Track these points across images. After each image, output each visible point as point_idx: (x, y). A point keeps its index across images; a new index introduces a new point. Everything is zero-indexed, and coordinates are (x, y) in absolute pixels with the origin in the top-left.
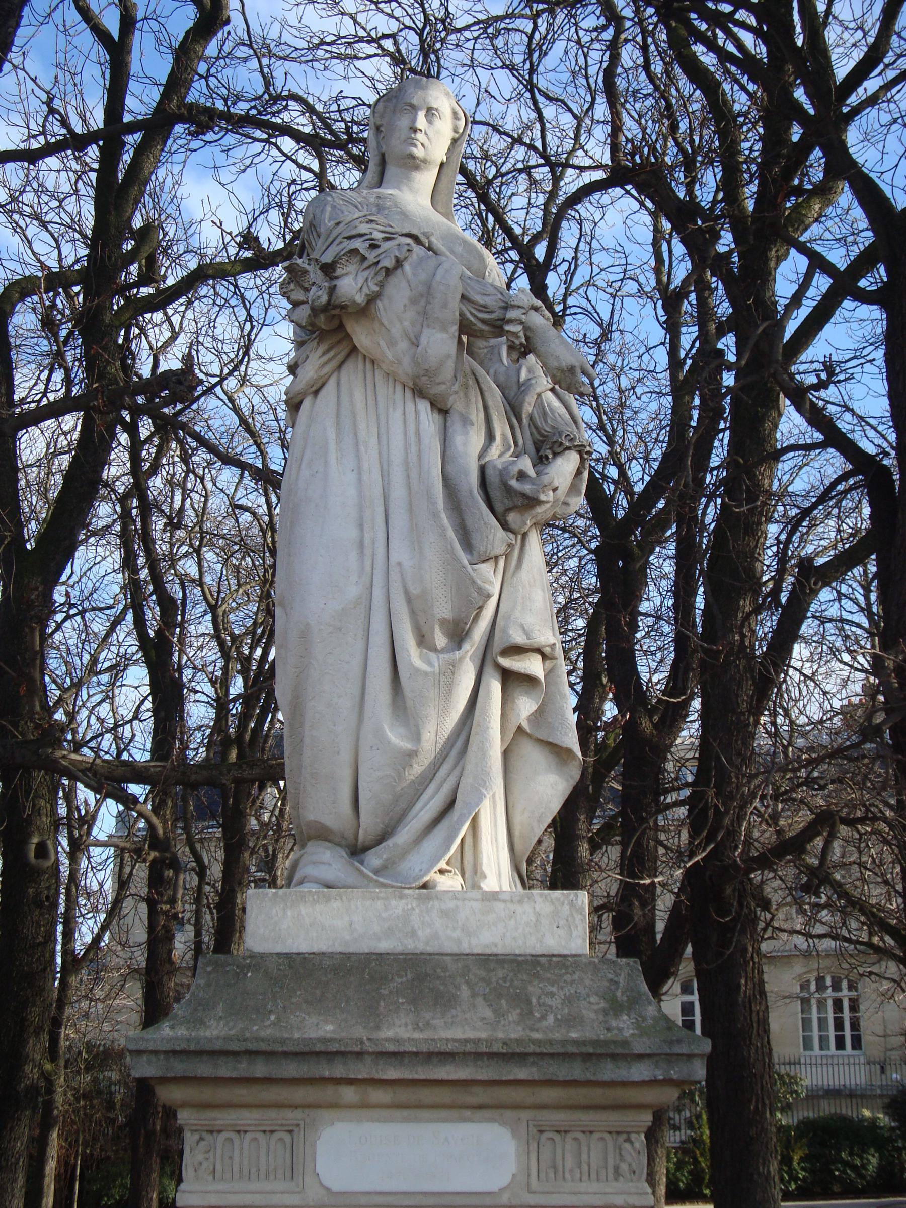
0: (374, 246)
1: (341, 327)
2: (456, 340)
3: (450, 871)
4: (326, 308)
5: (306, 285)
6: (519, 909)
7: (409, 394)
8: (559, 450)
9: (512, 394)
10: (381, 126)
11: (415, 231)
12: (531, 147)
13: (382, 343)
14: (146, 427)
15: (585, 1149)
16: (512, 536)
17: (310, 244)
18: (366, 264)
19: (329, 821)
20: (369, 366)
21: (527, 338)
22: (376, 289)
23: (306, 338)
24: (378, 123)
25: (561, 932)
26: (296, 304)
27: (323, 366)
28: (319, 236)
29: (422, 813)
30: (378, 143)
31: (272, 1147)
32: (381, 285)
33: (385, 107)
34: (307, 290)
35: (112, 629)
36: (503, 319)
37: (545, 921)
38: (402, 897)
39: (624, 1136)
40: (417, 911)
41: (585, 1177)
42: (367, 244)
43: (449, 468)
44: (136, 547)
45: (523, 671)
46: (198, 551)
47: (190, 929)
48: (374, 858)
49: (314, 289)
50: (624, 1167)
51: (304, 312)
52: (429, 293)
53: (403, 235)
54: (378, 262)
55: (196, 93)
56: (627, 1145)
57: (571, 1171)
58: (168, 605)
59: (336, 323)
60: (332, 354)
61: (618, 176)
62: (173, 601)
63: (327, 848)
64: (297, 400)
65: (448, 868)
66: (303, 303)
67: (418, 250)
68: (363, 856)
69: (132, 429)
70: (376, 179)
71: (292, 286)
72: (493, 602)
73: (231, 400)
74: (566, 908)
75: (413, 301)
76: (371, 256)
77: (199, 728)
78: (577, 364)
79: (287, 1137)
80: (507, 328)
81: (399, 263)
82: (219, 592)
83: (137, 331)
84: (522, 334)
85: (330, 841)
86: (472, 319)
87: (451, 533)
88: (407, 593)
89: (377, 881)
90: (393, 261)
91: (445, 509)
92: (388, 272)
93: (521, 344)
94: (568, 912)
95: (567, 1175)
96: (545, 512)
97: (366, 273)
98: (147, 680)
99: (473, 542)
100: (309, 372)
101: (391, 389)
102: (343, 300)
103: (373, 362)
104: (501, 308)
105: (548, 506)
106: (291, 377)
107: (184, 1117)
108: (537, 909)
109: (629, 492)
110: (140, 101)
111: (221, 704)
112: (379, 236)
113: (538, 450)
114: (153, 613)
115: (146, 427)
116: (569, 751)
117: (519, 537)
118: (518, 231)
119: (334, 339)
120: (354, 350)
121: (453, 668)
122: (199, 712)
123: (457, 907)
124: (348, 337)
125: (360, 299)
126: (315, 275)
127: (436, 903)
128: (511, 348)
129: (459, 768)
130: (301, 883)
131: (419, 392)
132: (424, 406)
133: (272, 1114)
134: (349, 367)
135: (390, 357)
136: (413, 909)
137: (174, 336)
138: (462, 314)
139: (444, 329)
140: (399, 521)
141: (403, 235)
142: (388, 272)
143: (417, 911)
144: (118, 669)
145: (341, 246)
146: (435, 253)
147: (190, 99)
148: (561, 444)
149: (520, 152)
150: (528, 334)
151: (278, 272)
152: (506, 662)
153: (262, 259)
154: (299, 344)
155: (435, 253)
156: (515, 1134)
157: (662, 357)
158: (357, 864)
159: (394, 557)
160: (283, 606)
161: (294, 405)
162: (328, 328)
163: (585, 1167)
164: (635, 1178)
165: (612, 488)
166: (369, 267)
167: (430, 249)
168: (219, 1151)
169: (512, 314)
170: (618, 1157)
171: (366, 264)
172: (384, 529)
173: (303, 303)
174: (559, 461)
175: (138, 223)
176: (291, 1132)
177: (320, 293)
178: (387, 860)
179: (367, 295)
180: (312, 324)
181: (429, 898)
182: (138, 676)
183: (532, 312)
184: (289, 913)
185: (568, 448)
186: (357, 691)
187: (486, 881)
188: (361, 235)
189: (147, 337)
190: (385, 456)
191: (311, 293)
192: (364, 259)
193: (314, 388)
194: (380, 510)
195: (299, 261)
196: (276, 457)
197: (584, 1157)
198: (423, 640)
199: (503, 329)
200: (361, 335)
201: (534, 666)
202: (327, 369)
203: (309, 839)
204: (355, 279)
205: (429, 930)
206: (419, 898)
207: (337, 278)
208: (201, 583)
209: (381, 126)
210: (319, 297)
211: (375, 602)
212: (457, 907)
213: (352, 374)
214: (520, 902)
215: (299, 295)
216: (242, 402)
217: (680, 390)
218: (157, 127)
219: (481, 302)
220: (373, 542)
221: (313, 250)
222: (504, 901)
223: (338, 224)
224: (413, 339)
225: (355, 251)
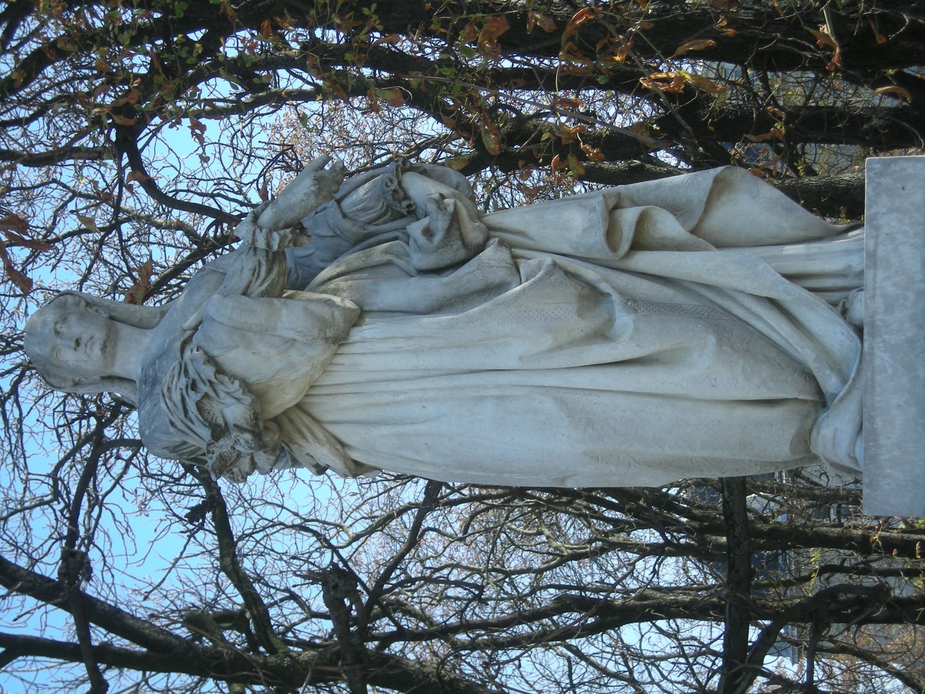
0: (194, 386)
1: (276, 420)
2: (289, 301)
3: (844, 304)
4: (258, 436)
5: (235, 456)
6: (885, 229)
7: (345, 349)
9: (344, 243)
10: (74, 381)
11: (178, 345)
12: (101, 242)
13: (292, 377)
14: (385, 626)
16: (492, 241)
17: (193, 452)
18: (212, 393)
19: (790, 432)
20: (315, 392)
21: (286, 226)
22: (237, 383)
23: (288, 456)
24: (71, 383)
26: (254, 466)
28: (185, 443)
29: (783, 334)
30: (91, 384)
32: (233, 377)
33: (55, 376)
34: (239, 455)
35: (583, 657)
36: (267, 252)
40: (886, 337)
42: (191, 393)
43: (421, 306)
44: (504, 635)
45: (634, 227)
46: (508, 574)
47: (891, 581)
48: (829, 383)
49: (238, 448)
51: (262, 458)
52: (241, 329)
53: (182, 356)
54: (210, 382)
55: (49, 568)
58: (562, 605)
59: (272, 425)
60: (304, 429)
61: (127, 144)
62: (558, 599)
63: (818, 433)
64: (352, 466)
65: (841, 304)
66: (252, 459)
67: (198, 338)
68: (827, 397)
69: (387, 639)
70: (127, 385)
71: (235, 470)
72: (560, 260)
73: (356, 538)
75: (249, 345)
76: (204, 388)
77: (686, 572)
78: (312, 175)
80: (275, 248)
82: (549, 554)
83: (290, 634)
84: (282, 232)
85: (811, 430)
86: (266, 284)
87: (487, 305)
89: (854, 380)
91: (462, 311)
96: (466, 207)
97: (222, 395)
98: (635, 625)
99: (497, 281)
100: (324, 454)
101: (339, 368)
102: (248, 415)
103: (312, 387)
104: (255, 254)
105: (459, 204)
106: (329, 472)
108: (884, 210)
109: (447, 139)
110: (58, 624)
111: (659, 551)
112: (183, 380)
113: (402, 216)
114: (571, 618)
115: (385, 626)
116: (717, 180)
117: (492, 233)
118: (186, 254)
119: (289, 427)
120: (299, 406)
122: (671, 572)
124: (285, 413)
125: (248, 399)
126: (224, 446)
127: (878, 317)
128: (295, 243)
129: (735, 295)
130: (855, 460)
131: (340, 340)
134: (315, 411)
135: (307, 368)
136: (884, 341)
137: (293, 597)
140: (476, 359)
141: (182, 356)
142: (220, 370)
143: (886, 337)
144: (628, 654)
145: (194, 418)
146: (201, 322)
147: (55, 576)
148: (395, 191)
149: (106, 253)
150: (281, 225)
151: (223, 483)
152: (625, 247)
153: (215, 504)
154: (295, 463)
155: (201, 322)
157: (312, 107)
158: (836, 401)
159: (513, 363)
160: (564, 480)
161: (356, 469)
162: (277, 436)
165: (444, 155)
166: (215, 391)
167: (196, 329)
169: (261, 244)
171: (212, 393)
172: (484, 374)
173: (252, 459)
174: (412, 193)
175: (183, 632)
177: (242, 441)
178: (831, 369)
179: (244, 393)
180: (274, 450)
181: (873, 324)
182: (630, 633)
184: (888, 471)
185: (400, 183)
186: (655, 401)
187: (854, 264)
188: (183, 400)
189: (295, 624)
190: (409, 374)
191: (242, 450)
193: (339, 447)
195: (210, 462)
196: (414, 492)
199: (277, 252)
200: (284, 399)
201: (629, 216)
202: (320, 434)
203: (808, 451)
204: (227, 406)
206: (873, 335)
207: (226, 424)
208: (540, 572)
209: (74, 381)
210: (247, 442)
211: (561, 384)
213: (328, 409)
214: (877, 228)
215: (245, 463)
216: (360, 527)
217: (341, 89)
218: (88, 611)
220: (497, 386)
221: (199, 449)
223: (172, 424)
224: (289, 344)
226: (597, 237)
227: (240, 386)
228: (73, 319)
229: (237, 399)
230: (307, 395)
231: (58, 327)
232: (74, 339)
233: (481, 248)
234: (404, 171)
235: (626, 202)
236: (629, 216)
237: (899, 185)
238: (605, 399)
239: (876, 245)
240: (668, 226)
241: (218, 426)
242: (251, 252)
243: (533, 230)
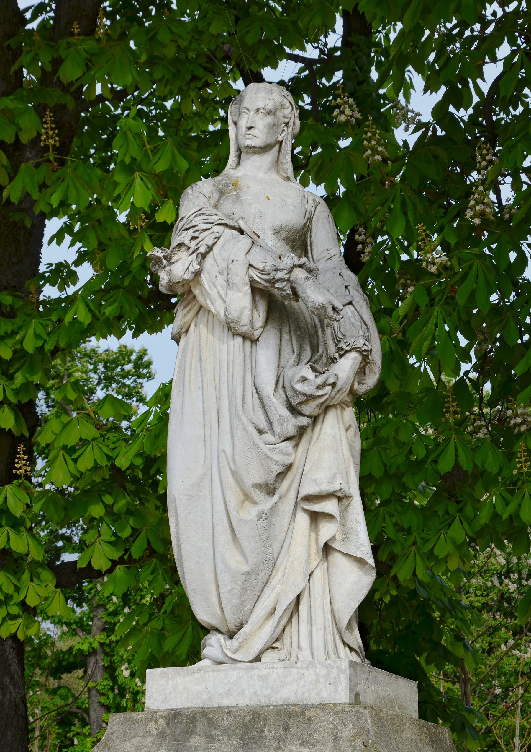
6: (306, 673)
18: (191, 251)
22: (198, 267)
25: (332, 687)
27: (185, 315)
37: (322, 680)
40: (245, 677)
60: (190, 307)
76: (193, 245)
78: (325, 302)
86: (258, 279)
88: (231, 469)
94: (335, 673)
108: (317, 671)
123: (269, 673)
127: (256, 671)
136: (243, 676)
142: (204, 256)
143: (245, 677)
148: (342, 349)
184: (170, 683)
192: (189, 248)
194: (215, 414)
201: (330, 506)
205: (252, 690)
212: (269, 673)
227: (196, 270)
228: (270, 119)
229: (188, 268)
231: (262, 110)
232: (253, 125)
235: (345, 502)
236: (330, 506)
238: (208, 505)
240: (327, 531)
241: (171, 258)
242: (275, 268)
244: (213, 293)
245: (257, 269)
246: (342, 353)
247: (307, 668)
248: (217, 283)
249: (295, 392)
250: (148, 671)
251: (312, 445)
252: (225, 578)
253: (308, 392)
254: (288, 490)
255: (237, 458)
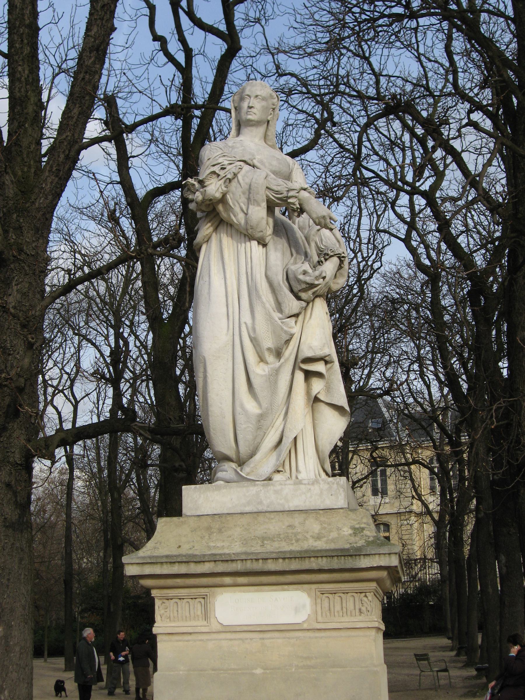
6: (312, 488)
8: (327, 257)
9: (306, 232)
15: (344, 601)
21: (300, 204)
31: (196, 606)
38: (255, 485)
39: (364, 594)
41: (345, 614)
43: (269, 273)
50: (363, 609)
56: (365, 599)
57: (338, 612)
67: (246, 168)
74: (335, 486)
79: (202, 601)
80: (289, 201)
81: (235, 175)
88: (250, 336)
90: (232, 174)
92: (230, 180)
93: (297, 208)
95: (336, 614)
107: (154, 593)
112: (226, 163)
121: (277, 372)
127: (272, 487)
132: (254, 243)
133: (193, 590)
138: (267, 196)
139: (259, 205)
142: (230, 180)
148: (328, 255)
156: (309, 595)
163: (345, 610)
164: (369, 614)
168: (171, 608)
170: (361, 605)
171: (220, 178)
176: (204, 598)
183: (302, 191)
192: (218, 175)
197: (344, 605)
198: (262, 359)
201: (319, 367)
205: (269, 500)
206: (263, 485)
219: (276, 189)
222: (305, 484)
225: (214, 173)
226: (309, 354)
228: (264, 103)
230: (227, 223)
233: (299, 298)
234: (339, 257)
235: (329, 366)
236: (319, 367)
237: (333, 493)
239: (305, 484)
240: (317, 386)
243: (312, 321)
244: (237, 209)
245: (273, 190)
246: (327, 257)
247: (313, 484)
248: (240, 201)
249: (299, 281)
250: (183, 487)
251: (306, 322)
252: (241, 419)
253: (310, 282)
254: (291, 354)
255: (257, 328)
